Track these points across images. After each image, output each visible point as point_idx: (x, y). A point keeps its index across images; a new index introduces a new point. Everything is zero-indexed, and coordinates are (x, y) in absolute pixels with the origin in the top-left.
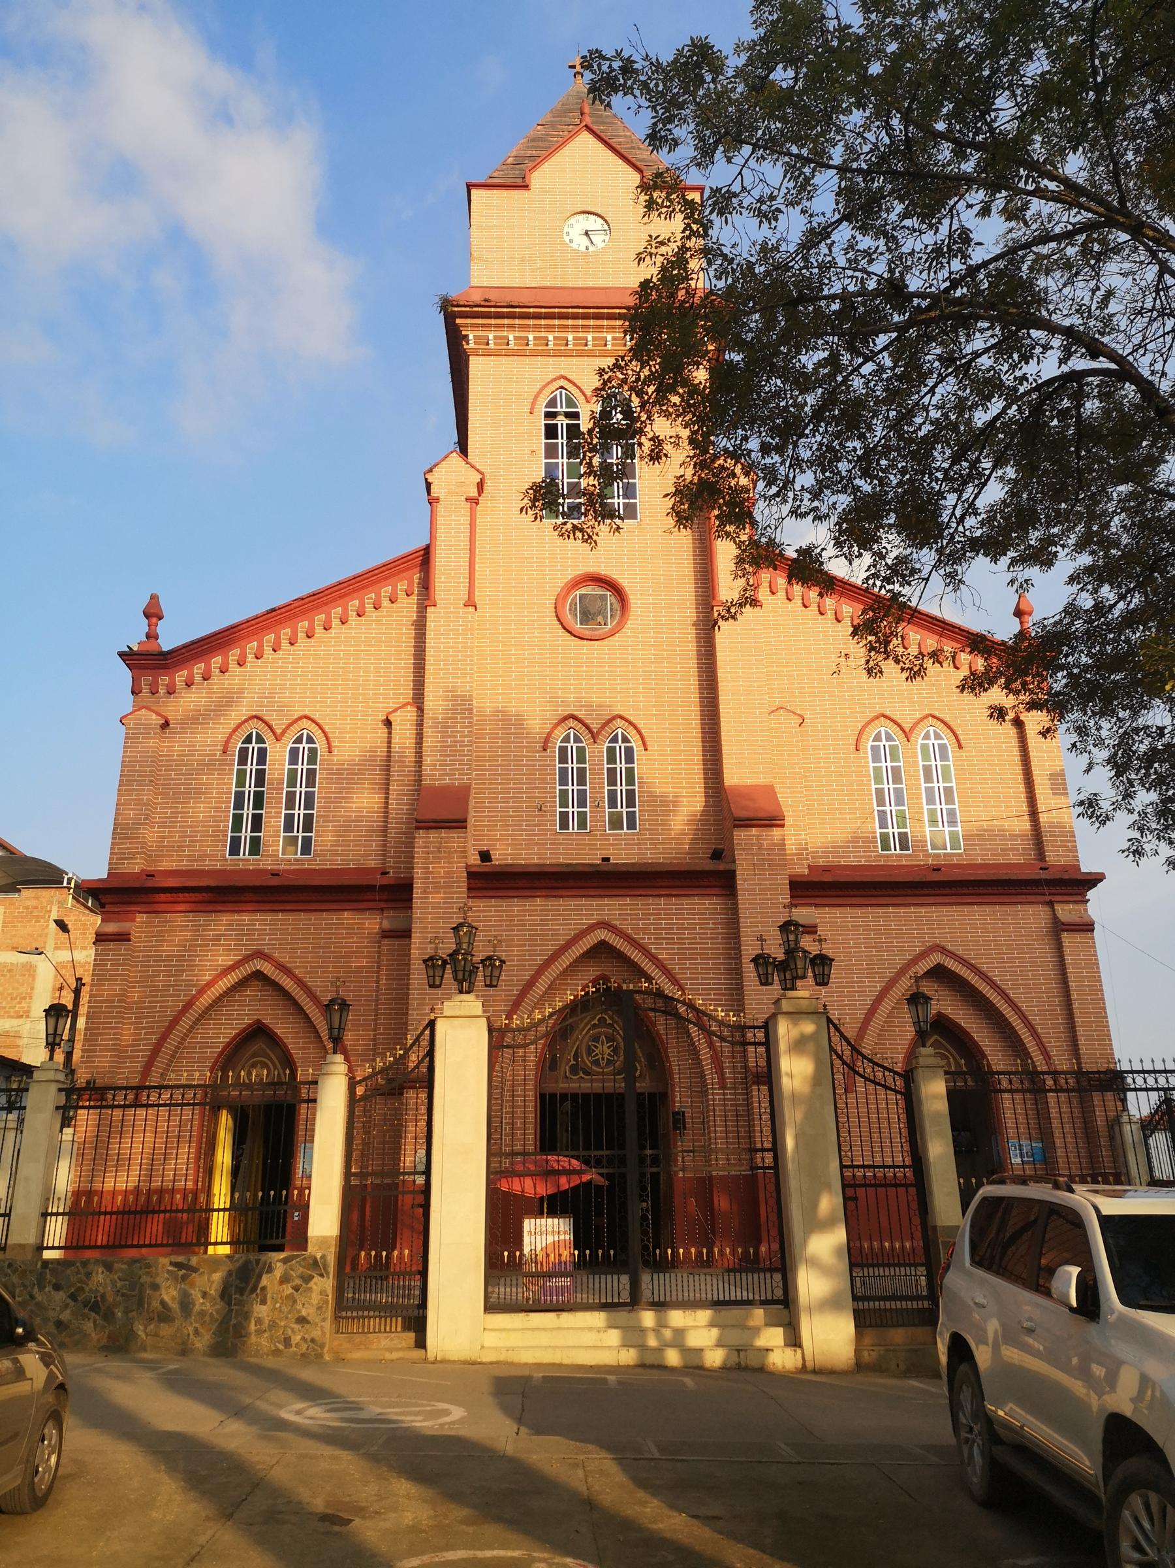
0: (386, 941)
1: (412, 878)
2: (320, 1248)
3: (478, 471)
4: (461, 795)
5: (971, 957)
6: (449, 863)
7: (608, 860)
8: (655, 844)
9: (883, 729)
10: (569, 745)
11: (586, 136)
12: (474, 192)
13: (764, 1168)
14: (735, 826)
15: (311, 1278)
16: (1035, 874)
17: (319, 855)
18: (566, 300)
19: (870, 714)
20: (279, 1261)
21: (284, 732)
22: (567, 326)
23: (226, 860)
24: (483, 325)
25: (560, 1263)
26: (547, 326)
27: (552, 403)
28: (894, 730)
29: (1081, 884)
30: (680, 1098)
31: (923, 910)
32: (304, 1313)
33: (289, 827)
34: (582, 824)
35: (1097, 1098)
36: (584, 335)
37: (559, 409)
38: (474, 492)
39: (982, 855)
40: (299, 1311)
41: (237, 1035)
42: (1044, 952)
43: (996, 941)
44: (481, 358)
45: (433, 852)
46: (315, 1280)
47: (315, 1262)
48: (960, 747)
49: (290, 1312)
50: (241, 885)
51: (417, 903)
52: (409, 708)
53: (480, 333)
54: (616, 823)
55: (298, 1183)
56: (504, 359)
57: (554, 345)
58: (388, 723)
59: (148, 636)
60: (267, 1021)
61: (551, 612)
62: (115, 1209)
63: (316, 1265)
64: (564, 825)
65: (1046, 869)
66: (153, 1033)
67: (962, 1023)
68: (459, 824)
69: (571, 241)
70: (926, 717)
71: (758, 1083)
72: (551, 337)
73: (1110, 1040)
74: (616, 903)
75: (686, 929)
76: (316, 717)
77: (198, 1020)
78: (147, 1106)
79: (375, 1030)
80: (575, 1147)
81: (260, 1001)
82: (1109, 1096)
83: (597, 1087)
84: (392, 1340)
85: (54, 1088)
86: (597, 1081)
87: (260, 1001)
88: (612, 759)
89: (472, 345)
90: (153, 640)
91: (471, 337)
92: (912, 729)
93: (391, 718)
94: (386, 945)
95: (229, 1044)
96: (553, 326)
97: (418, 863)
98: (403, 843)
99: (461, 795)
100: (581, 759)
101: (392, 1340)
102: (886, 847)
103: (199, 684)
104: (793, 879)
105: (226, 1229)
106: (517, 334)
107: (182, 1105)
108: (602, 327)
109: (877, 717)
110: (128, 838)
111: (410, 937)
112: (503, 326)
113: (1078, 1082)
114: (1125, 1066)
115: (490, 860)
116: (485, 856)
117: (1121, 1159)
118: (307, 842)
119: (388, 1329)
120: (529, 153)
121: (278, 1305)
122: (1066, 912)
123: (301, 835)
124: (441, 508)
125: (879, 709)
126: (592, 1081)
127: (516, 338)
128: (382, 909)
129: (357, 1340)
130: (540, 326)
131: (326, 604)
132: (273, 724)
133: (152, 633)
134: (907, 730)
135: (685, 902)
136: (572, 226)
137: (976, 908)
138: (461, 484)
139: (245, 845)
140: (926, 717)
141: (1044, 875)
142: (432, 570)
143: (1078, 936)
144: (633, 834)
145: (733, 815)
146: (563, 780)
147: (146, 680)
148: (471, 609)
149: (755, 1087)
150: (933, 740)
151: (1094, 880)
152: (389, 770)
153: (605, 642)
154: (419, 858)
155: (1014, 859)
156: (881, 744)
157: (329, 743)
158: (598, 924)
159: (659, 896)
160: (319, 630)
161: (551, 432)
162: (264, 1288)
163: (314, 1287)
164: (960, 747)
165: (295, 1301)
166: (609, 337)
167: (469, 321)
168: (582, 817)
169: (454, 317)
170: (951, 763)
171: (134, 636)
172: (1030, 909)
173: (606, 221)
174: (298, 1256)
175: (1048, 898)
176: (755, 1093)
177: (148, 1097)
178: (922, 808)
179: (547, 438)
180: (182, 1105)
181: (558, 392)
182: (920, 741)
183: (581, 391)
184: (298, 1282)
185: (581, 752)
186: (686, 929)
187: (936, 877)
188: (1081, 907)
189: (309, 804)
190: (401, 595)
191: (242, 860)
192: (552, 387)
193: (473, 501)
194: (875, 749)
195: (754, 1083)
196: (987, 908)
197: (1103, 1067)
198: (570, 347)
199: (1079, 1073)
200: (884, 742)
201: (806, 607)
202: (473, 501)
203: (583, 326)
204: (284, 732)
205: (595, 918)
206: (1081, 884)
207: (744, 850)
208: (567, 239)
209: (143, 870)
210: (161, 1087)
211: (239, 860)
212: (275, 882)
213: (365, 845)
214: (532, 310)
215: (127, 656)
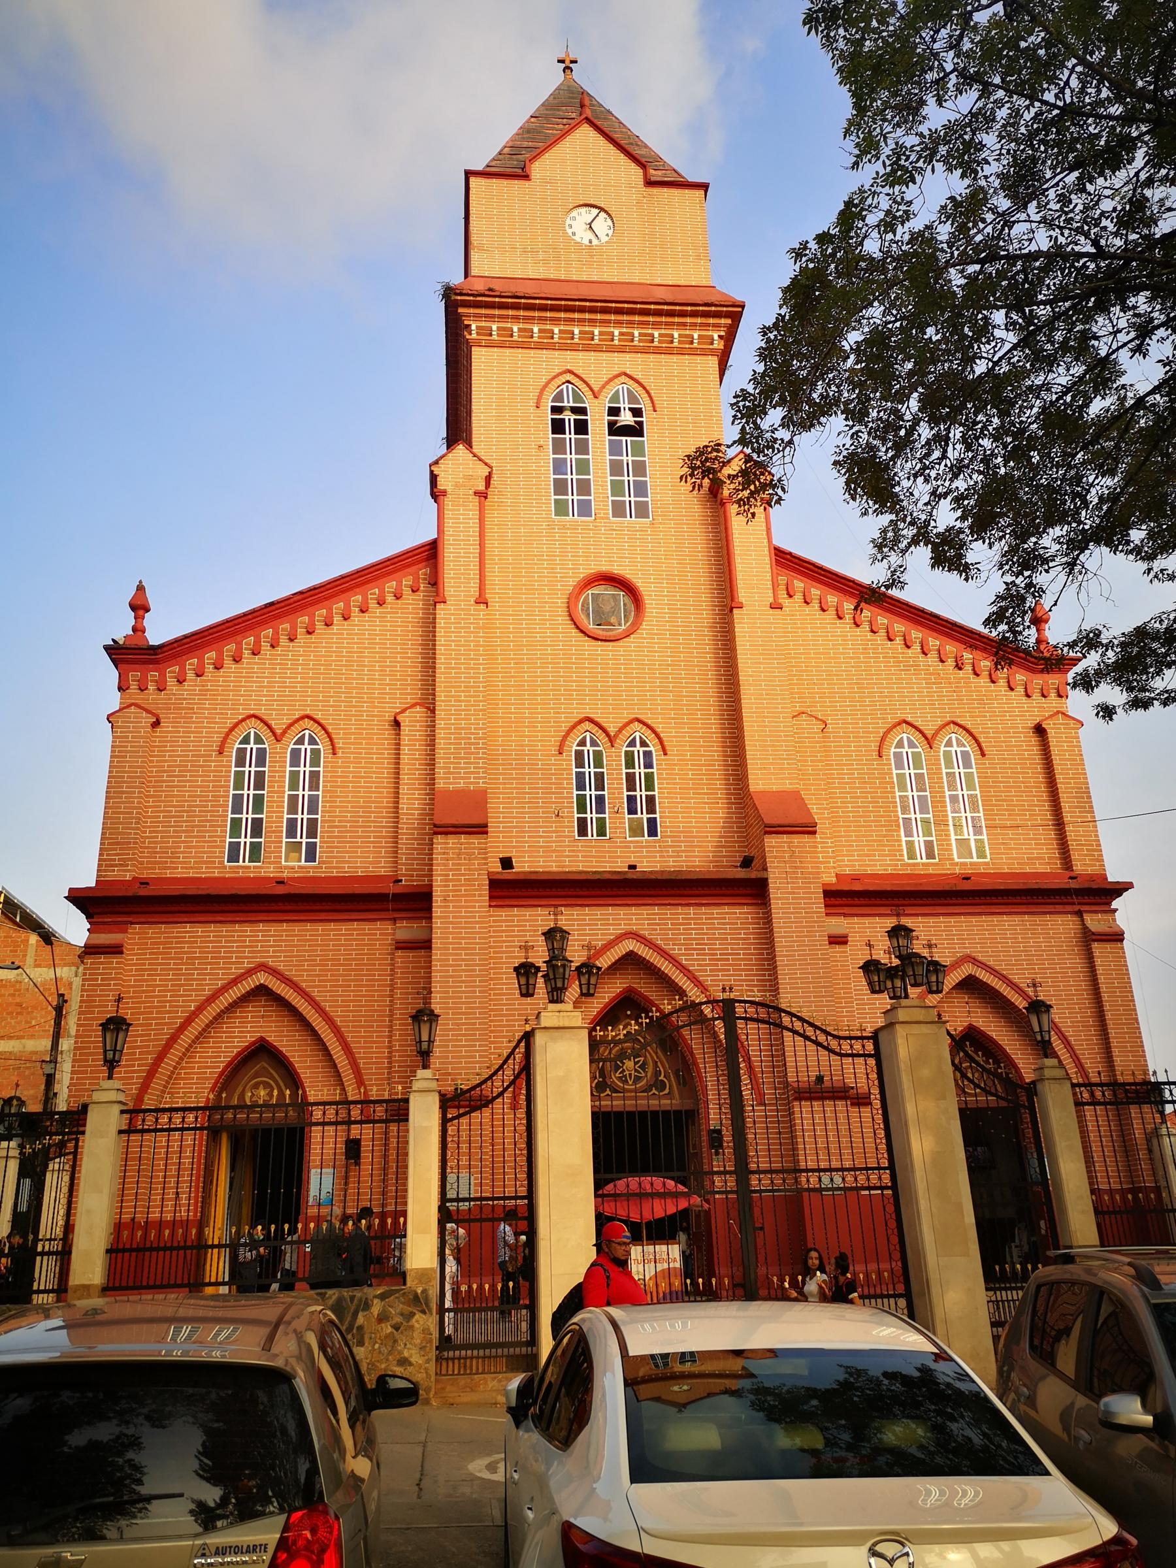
0: (399, 953)
1: (431, 886)
2: (420, 1282)
3: (486, 464)
4: (479, 799)
5: (1001, 967)
6: (469, 870)
7: (634, 867)
8: (678, 852)
9: (905, 735)
10: (585, 749)
11: (586, 129)
12: (472, 180)
13: (760, 1191)
14: (766, 833)
15: (412, 1314)
16: (1063, 883)
17: (324, 862)
18: (573, 292)
19: (891, 720)
20: (375, 1297)
21: (285, 732)
22: (573, 320)
23: (225, 867)
24: (487, 316)
25: (671, 1292)
26: (552, 319)
27: (559, 397)
28: (916, 737)
29: (1104, 893)
30: (715, 1115)
31: (952, 920)
32: (406, 1354)
33: (291, 832)
34: (601, 832)
35: (1134, 1110)
36: (591, 329)
37: (565, 404)
38: (481, 487)
39: (1009, 864)
40: (400, 1353)
41: (239, 1054)
42: (1074, 963)
43: (1025, 951)
44: (484, 349)
45: (453, 859)
46: (417, 1317)
47: (416, 1297)
48: (983, 755)
49: (390, 1353)
50: (226, 893)
51: (437, 912)
52: (418, 709)
53: (483, 324)
54: (636, 830)
55: (312, 1212)
56: (508, 351)
57: (560, 338)
58: (397, 724)
59: (134, 629)
60: (271, 1038)
61: (562, 611)
62: (134, 1246)
63: (418, 1302)
64: (582, 831)
65: (1075, 878)
66: (149, 1053)
67: (994, 1035)
68: (480, 829)
69: (574, 234)
70: (948, 724)
71: (800, 1099)
72: (556, 330)
73: (1143, 1051)
74: (644, 912)
75: (717, 939)
76: (318, 716)
77: (197, 1038)
78: (143, 1131)
79: (390, 1047)
80: (669, 1168)
81: (263, 1017)
82: (1146, 1108)
83: (630, 1105)
84: (500, 1381)
85: (116, 1109)
86: (630, 1098)
87: (263, 1017)
88: (630, 763)
89: (474, 336)
90: (140, 633)
91: (473, 327)
92: (935, 735)
93: (399, 718)
94: (400, 957)
95: (230, 1063)
96: (559, 319)
97: (437, 870)
98: (415, 849)
99: (479, 799)
100: (598, 763)
101: (500, 1381)
102: (912, 855)
103: (191, 680)
104: (828, 888)
105: (37, 1275)
106: (521, 326)
107: (182, 1129)
108: (609, 321)
109: (899, 724)
110: (118, 843)
111: (430, 948)
112: (507, 317)
113: (1115, 1095)
114: (1162, 1078)
115: (512, 867)
116: (507, 863)
117: (1161, 1173)
118: (311, 848)
119: (444, 1372)
120: (525, 144)
121: (377, 1346)
122: (1094, 922)
123: (304, 840)
124: (448, 502)
125: (900, 716)
126: (624, 1098)
127: (520, 330)
128: (395, 920)
129: (463, 1382)
130: (546, 319)
131: (327, 599)
132: (273, 723)
133: (139, 626)
134: (929, 737)
135: (715, 911)
136: (574, 219)
137: (1005, 918)
138: (469, 478)
139: (245, 852)
140: (948, 724)
141: (1073, 885)
142: (440, 565)
143: (1108, 946)
144: (655, 842)
145: (761, 822)
146: (581, 786)
147: (134, 676)
148: (482, 606)
149: (796, 1103)
150: (955, 748)
151: (1120, 889)
152: (398, 773)
153: (621, 643)
154: (438, 865)
155: (1040, 868)
156: (904, 751)
157: (333, 744)
158: (625, 934)
159: (688, 905)
160: (320, 626)
161: (558, 427)
162: (360, 1328)
163: (417, 1325)
164: (983, 755)
165: (395, 1341)
166: (616, 333)
167: (472, 311)
168: (601, 824)
169: (456, 304)
170: (974, 770)
171: (121, 628)
172: (1060, 919)
173: (609, 215)
174: (397, 1291)
175: (1076, 908)
176: (797, 1109)
177: (144, 1120)
178: (947, 816)
179: (553, 433)
180: (182, 1129)
181: (564, 386)
182: (942, 749)
183: (588, 385)
184: (399, 1319)
185: (598, 756)
186: (717, 939)
187: (967, 886)
188: (1108, 917)
189: (313, 809)
190: (406, 591)
191: (242, 867)
192: (559, 381)
193: (482, 495)
194: (898, 756)
195: (796, 1099)
196: (1017, 918)
197: (1140, 1078)
198: (576, 340)
199: (1114, 1085)
200: (906, 749)
201: (823, 610)
202: (482, 495)
203: (590, 320)
204: (285, 732)
205: (623, 928)
206: (1104, 893)
207: (776, 857)
208: (570, 231)
209: (134, 878)
210: (157, 1110)
211: (238, 867)
212: (280, 890)
213: (374, 852)
214: (537, 302)
215: (116, 652)
